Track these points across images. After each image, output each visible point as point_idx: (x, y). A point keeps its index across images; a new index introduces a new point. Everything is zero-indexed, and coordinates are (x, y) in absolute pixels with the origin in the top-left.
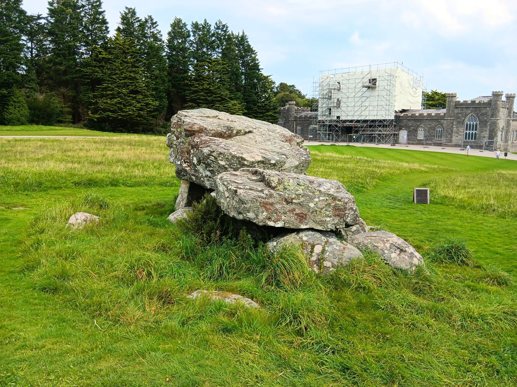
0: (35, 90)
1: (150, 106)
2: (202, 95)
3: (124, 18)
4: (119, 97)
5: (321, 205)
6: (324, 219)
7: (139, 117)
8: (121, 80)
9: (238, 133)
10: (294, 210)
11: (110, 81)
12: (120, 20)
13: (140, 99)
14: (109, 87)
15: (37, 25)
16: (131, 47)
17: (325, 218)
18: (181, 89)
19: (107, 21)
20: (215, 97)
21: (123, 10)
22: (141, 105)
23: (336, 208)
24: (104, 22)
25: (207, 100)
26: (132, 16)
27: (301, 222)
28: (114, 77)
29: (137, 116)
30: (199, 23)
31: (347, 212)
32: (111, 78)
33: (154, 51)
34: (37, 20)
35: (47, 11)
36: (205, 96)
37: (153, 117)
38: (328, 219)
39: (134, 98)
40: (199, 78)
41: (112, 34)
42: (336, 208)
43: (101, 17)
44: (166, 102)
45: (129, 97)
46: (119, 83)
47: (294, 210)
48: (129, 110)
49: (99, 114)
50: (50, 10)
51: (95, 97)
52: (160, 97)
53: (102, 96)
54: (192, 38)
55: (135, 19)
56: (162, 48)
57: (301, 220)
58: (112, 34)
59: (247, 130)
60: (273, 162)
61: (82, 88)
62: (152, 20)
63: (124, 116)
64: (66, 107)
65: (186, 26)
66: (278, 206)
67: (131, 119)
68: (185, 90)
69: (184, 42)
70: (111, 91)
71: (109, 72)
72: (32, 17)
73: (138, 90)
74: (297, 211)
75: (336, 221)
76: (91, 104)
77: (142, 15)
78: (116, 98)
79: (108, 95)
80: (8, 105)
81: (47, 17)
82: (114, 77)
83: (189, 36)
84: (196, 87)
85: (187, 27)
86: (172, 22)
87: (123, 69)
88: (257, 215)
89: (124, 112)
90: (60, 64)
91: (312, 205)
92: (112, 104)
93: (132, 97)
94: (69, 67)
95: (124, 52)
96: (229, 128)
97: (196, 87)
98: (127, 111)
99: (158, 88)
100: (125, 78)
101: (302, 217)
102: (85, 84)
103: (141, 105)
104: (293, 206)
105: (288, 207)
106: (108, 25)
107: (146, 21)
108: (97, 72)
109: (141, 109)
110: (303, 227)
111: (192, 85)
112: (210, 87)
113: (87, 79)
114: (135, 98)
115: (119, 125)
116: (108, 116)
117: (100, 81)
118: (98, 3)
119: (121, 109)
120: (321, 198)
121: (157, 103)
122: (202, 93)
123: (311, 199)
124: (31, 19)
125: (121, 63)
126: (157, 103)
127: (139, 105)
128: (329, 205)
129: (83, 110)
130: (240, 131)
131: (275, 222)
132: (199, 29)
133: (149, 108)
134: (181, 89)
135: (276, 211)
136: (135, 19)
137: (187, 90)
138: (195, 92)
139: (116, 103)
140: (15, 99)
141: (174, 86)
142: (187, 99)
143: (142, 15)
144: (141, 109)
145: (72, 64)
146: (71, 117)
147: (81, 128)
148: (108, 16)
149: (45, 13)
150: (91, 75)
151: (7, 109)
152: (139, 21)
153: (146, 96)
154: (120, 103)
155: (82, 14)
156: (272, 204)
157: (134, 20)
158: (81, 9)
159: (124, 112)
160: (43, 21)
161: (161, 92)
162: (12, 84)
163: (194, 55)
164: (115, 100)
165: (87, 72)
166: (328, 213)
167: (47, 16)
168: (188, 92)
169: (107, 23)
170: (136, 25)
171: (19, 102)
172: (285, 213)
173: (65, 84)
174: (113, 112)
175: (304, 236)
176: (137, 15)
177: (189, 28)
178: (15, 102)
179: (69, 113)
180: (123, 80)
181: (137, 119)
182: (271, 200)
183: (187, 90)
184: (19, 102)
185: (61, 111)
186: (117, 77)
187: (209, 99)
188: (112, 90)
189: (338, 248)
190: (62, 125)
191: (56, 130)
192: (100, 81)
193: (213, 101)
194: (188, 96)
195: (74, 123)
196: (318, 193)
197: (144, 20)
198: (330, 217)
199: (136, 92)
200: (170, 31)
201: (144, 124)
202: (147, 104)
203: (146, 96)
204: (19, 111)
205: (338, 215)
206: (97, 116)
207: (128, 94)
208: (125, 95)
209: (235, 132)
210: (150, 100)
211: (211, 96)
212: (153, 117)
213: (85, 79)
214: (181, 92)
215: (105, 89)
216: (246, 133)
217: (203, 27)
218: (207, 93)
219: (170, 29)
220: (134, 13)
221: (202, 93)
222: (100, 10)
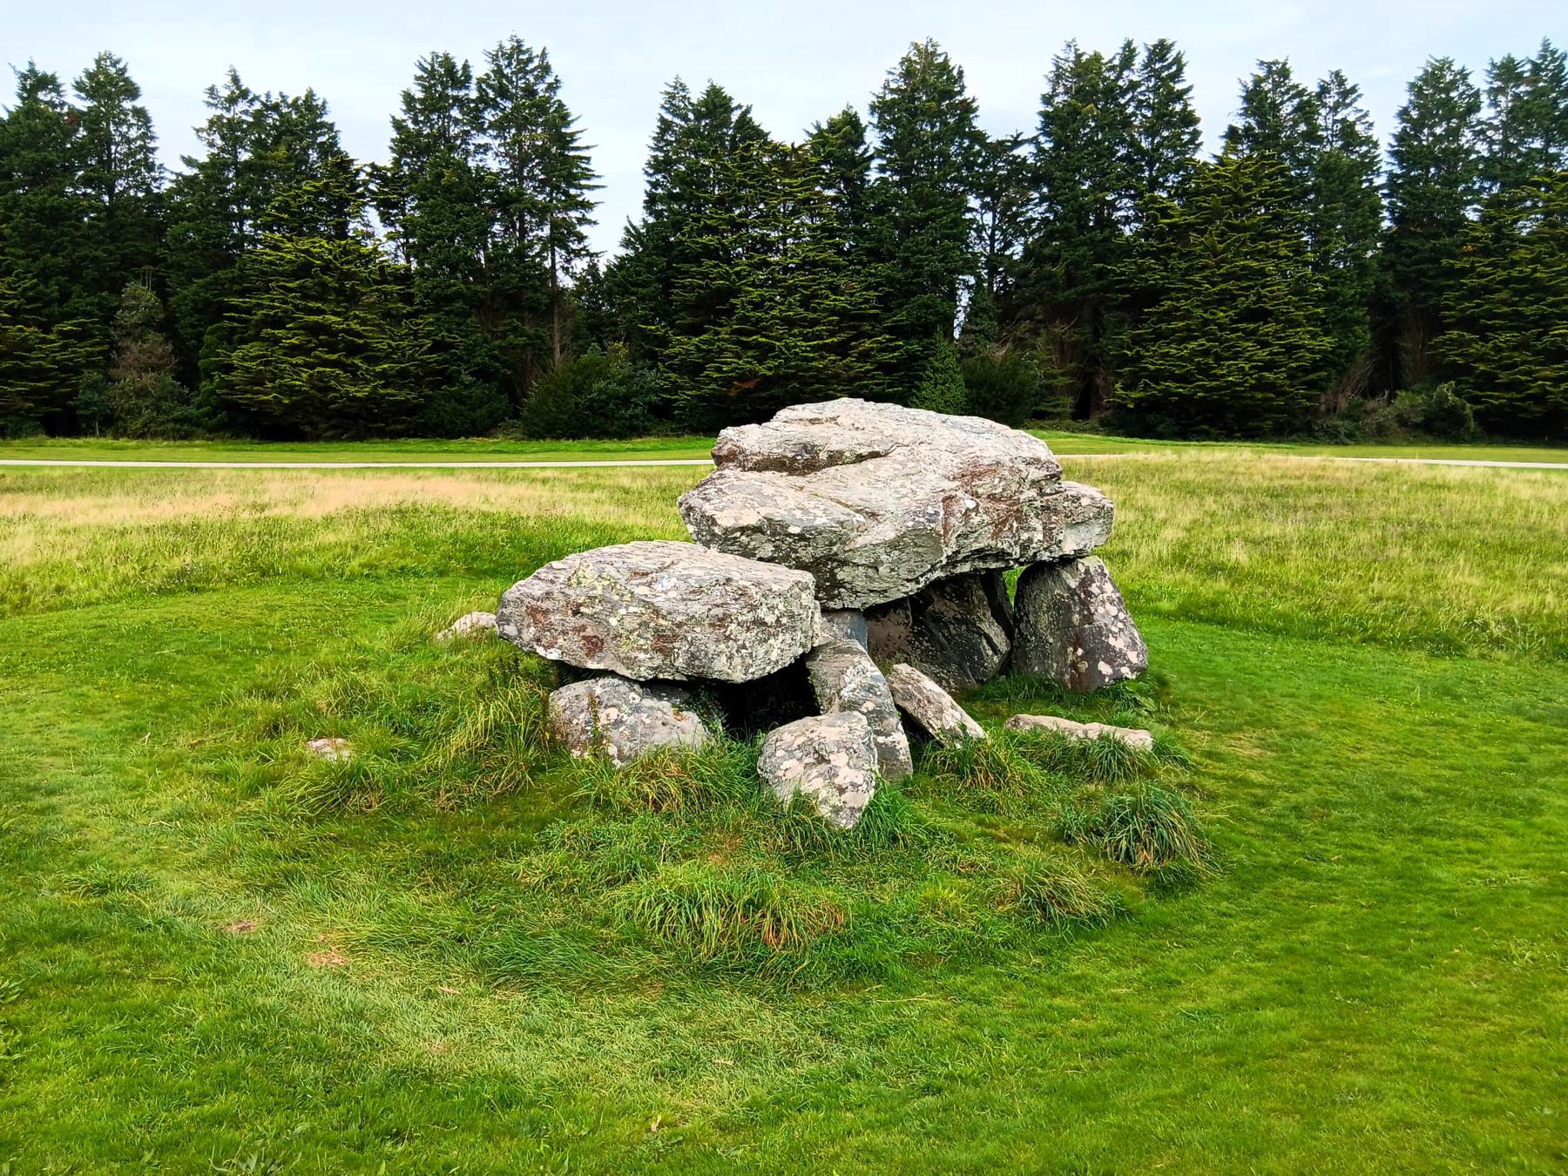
0: (987, 338)
1: (1302, 353)
2: (1504, 303)
3: (1256, 100)
4: (1204, 334)
5: (631, 623)
6: (633, 655)
7: (1263, 392)
8: (1213, 284)
9: (835, 459)
10: (584, 628)
11: (1185, 290)
12: (1239, 104)
13: (1267, 334)
14: (1177, 309)
15: (1010, 163)
16: (1261, 180)
17: (636, 654)
18: (1426, 287)
19: (1197, 114)
20: (1551, 305)
21: (1249, 71)
22: (1271, 354)
23: (659, 635)
24: (1189, 119)
25: (1521, 315)
26: (1276, 85)
27: (590, 654)
28: (1197, 278)
29: (1253, 388)
30: (1518, 57)
31: (677, 645)
32: (1190, 282)
33: (1343, 175)
34: (1012, 148)
35: (1038, 121)
36: (1515, 304)
37: (1312, 385)
38: (642, 656)
39: (1249, 334)
40: (1499, 240)
41: (1210, 149)
42: (659, 635)
43: (1178, 107)
44: (1364, 336)
45: (1234, 331)
46: (1209, 295)
47: (584, 628)
48: (1230, 373)
49: (1144, 390)
50: (1045, 115)
51: (1137, 341)
52: (1344, 320)
53: (1159, 336)
54: (1486, 113)
55: (1287, 92)
56: (1369, 165)
57: (590, 650)
58: (1210, 149)
59: (864, 451)
60: (794, 530)
61: (1110, 317)
62: (1341, 82)
63: (1212, 389)
64: (1062, 375)
65: (1465, 77)
66: (554, 618)
67: (1236, 396)
68: (1440, 291)
69: (1454, 133)
70: (1182, 318)
71: (1184, 265)
72: (1001, 143)
73: (1266, 306)
74: (589, 632)
75: (657, 662)
76: (1126, 361)
77: (1307, 78)
78: (1196, 338)
79: (1174, 331)
80: (920, 379)
81: (1036, 138)
82: (1197, 278)
83: (1474, 108)
84: (1481, 275)
85: (1470, 80)
86: (1415, 73)
87: (1225, 251)
88: (520, 631)
89: (1216, 377)
90: (1054, 260)
91: (613, 621)
92: (1181, 358)
93: (1243, 330)
94: (1076, 264)
95: (1238, 199)
96: (807, 448)
97: (1481, 275)
98: (1223, 376)
99: (1338, 294)
100: (1226, 277)
101: (594, 646)
102: (1118, 308)
103: (1271, 354)
104: (584, 621)
105: (573, 621)
106: (1199, 127)
107: (1324, 90)
108: (1150, 269)
109: (1269, 366)
110: (592, 665)
111: (1464, 272)
112: (1535, 270)
113: (1122, 291)
114: (1254, 332)
115: (1198, 418)
116: (1167, 393)
117: (1153, 295)
118: (1174, 68)
119: (1205, 371)
120: (632, 609)
121: (1327, 342)
122: (1504, 295)
123: (613, 609)
124: (1001, 148)
125: (1222, 234)
126: (1327, 342)
127: (1263, 354)
128: (644, 624)
129: (1105, 379)
130: (841, 453)
131: (546, 648)
132: (1519, 79)
133: (1297, 360)
134: (1426, 287)
135: (549, 627)
136: (1287, 92)
137: (1450, 287)
138: (1473, 293)
139: (1194, 353)
140: (936, 364)
141: (1403, 281)
142: (1445, 317)
143: (1307, 78)
144: (1269, 366)
145: (1084, 256)
146: (1070, 400)
147: (1094, 431)
148: (1196, 104)
149: (1030, 125)
150: (1131, 281)
151: (918, 388)
152: (1300, 94)
153: (1293, 323)
154: (1206, 353)
155: (1130, 110)
156: (546, 612)
157: (1283, 94)
158: (1128, 97)
159: (1216, 377)
160: (1024, 151)
161: (1350, 304)
162: (934, 326)
163: (1493, 168)
164: (1193, 345)
165: (1123, 273)
166: (642, 642)
167: (1036, 133)
168: (1452, 294)
169: (1196, 121)
170: (1287, 109)
171: (944, 371)
172: (564, 633)
173: (1063, 311)
174: (1184, 379)
175: (599, 687)
176: (1294, 79)
177: (1480, 81)
178: (936, 370)
179: (1069, 390)
180: (1224, 282)
181: (1252, 398)
182: (546, 605)
183: (1450, 287)
184: (944, 371)
185: (1048, 387)
186: (1204, 278)
187: (1529, 310)
188: (1187, 315)
189: (648, 721)
190: (1045, 423)
191: (47, 486)
192: (1153, 295)
193: (1543, 317)
194: (1452, 309)
195: (1075, 417)
196: (627, 598)
197: (1313, 89)
198: (646, 651)
199: (1261, 315)
200: (1405, 104)
201: (1279, 410)
202: (1290, 349)
203: (1293, 323)
204: (943, 393)
205: (660, 650)
206: (1135, 395)
207: (1235, 322)
208: (1221, 328)
209: (823, 456)
210: (1302, 336)
211: (1537, 301)
212: (1312, 385)
213: (1118, 291)
214: (1426, 299)
215: (1168, 316)
216: (860, 458)
217: (1536, 68)
218: (1522, 293)
219: (1404, 99)
220: (1284, 73)
221: (1504, 295)
222: (1179, 87)
